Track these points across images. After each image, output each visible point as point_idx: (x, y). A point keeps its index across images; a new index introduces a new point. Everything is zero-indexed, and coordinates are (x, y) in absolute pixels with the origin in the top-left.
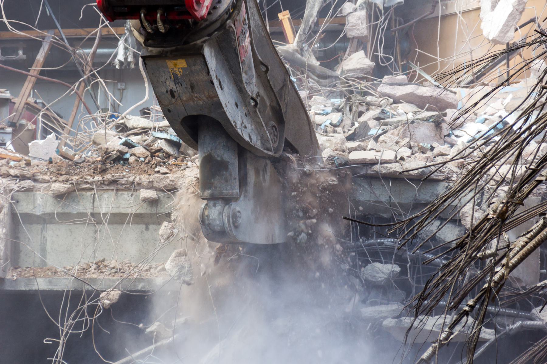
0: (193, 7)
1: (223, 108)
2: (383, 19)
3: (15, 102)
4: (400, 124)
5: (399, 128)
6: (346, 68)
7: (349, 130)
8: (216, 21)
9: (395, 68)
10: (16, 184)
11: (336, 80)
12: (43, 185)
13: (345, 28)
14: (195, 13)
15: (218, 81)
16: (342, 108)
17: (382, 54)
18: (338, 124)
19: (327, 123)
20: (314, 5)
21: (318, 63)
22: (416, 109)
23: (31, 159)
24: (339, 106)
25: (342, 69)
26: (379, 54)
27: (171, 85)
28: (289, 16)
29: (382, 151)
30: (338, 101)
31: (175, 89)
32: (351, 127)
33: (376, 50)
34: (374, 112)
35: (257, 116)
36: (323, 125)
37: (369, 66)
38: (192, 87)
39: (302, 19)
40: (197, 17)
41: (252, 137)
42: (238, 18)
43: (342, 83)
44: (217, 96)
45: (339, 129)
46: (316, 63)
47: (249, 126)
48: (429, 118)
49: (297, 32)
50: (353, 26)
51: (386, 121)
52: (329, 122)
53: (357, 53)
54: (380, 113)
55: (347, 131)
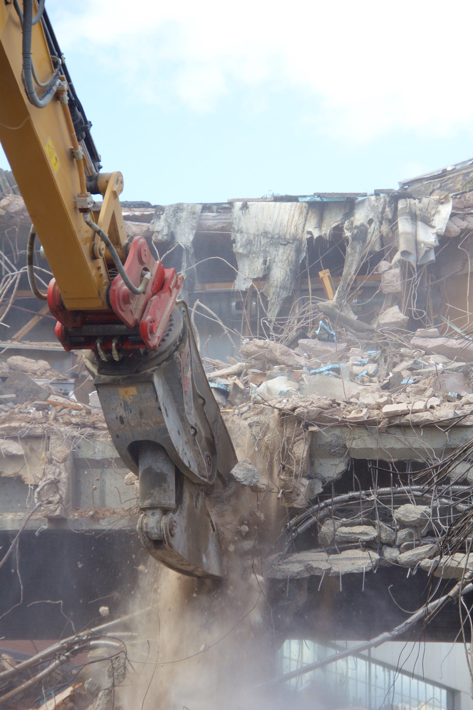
0: (147, 336)
1: (168, 433)
2: (416, 275)
3: (77, 354)
4: (431, 374)
5: (430, 378)
6: (382, 322)
7: (384, 380)
8: (165, 351)
9: (428, 321)
10: (77, 431)
11: (372, 333)
12: (102, 432)
13: (381, 284)
14: (149, 342)
15: (164, 408)
16: (378, 359)
17: (415, 309)
18: (374, 374)
19: (364, 374)
20: (352, 263)
21: (356, 317)
22: (446, 360)
23: (91, 408)
24: (375, 357)
25: (378, 323)
26: (412, 309)
27: (121, 412)
28: (329, 274)
29: (413, 402)
30: (373, 353)
31: (124, 415)
32: (386, 377)
33: (410, 306)
34: (405, 364)
35: (195, 444)
36: (360, 375)
37: (403, 320)
38: (141, 414)
39: (341, 276)
40: (150, 346)
41: (191, 464)
42: (184, 350)
43: (378, 336)
44: (164, 422)
45: (375, 379)
46: (354, 317)
47: (188, 453)
48: (458, 369)
49: (336, 289)
50: (388, 283)
51: (418, 371)
52: (366, 372)
53: (392, 308)
54: (412, 364)
55: (382, 380)
